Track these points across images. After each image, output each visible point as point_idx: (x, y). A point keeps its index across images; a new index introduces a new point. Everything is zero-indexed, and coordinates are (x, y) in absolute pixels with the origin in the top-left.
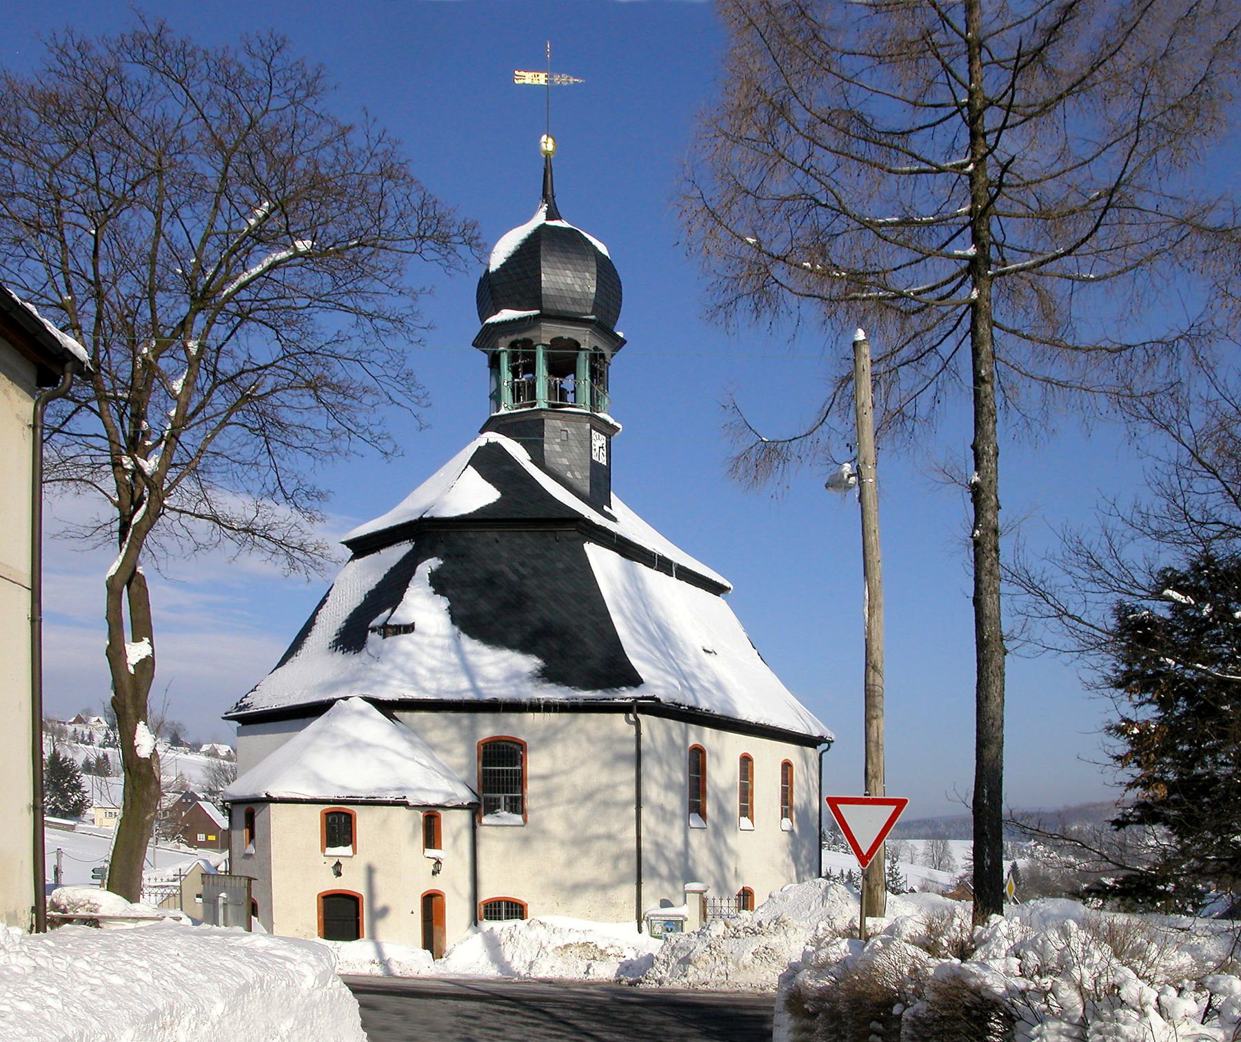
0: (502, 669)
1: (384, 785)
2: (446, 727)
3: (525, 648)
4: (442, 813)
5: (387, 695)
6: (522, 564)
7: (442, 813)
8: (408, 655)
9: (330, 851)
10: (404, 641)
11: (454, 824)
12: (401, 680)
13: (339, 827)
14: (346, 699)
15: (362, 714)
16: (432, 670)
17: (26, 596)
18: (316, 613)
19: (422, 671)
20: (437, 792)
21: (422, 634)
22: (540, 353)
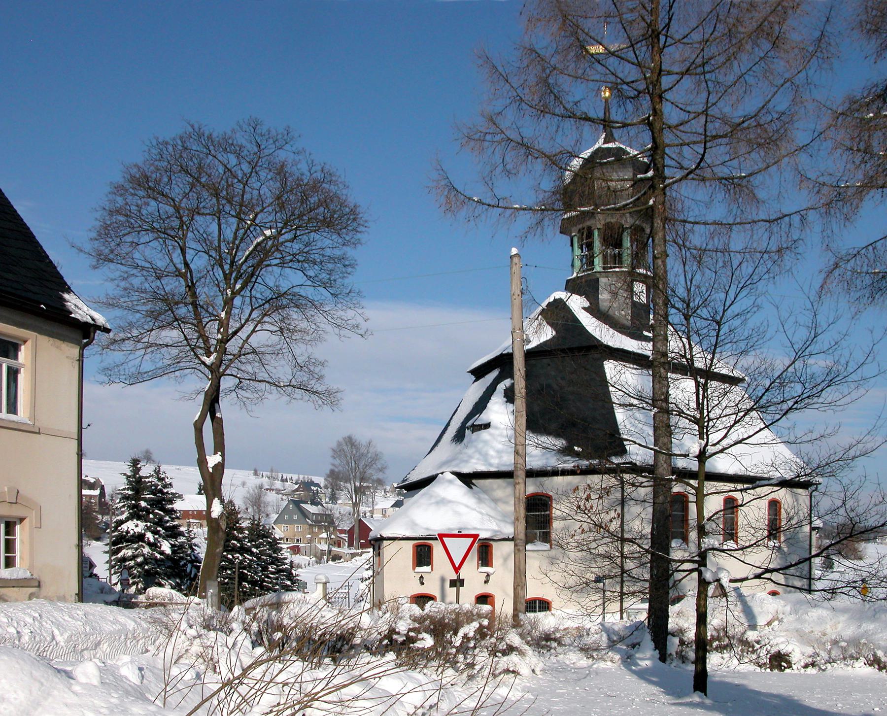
0: (541, 451)
1: (452, 527)
2: (505, 488)
3: (557, 435)
4: (494, 544)
5: (466, 469)
6: (563, 379)
7: (494, 544)
8: (486, 442)
9: (418, 569)
10: (484, 434)
11: (502, 552)
12: (478, 459)
13: (423, 555)
14: (442, 473)
15: (450, 482)
16: (498, 452)
17: (75, 443)
18: (451, 418)
19: (492, 453)
20: (486, 530)
21: (496, 428)
22: (596, 233)
